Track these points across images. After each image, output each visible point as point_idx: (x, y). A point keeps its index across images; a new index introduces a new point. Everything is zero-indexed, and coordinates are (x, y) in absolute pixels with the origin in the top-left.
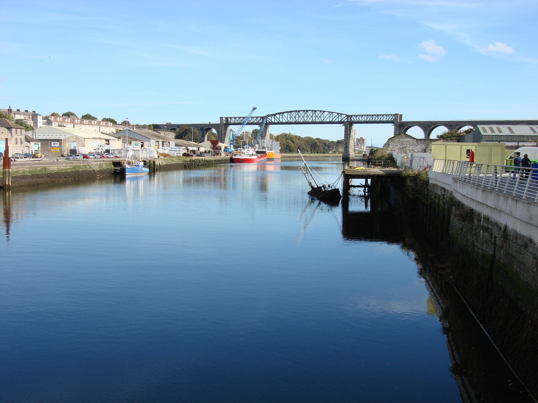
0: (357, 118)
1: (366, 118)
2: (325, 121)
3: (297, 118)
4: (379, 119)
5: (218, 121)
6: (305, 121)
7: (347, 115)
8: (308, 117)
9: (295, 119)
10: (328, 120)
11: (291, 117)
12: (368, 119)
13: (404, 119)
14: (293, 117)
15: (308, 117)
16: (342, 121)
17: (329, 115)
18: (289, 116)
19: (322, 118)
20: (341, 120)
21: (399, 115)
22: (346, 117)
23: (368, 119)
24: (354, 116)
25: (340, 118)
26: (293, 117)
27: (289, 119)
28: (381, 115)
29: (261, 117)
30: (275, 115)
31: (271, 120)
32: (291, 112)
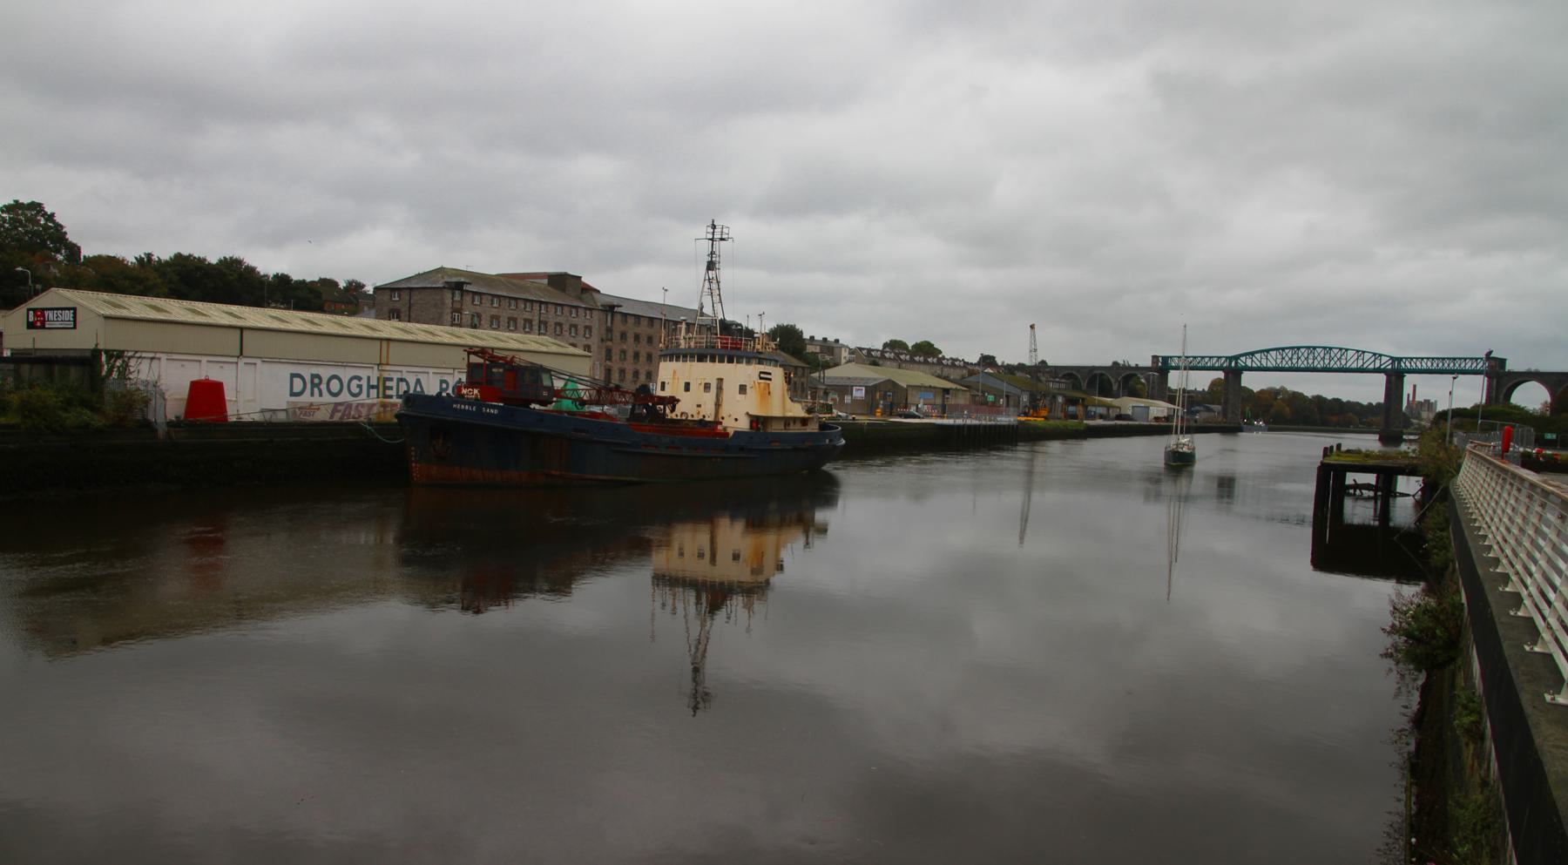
0: (1423, 364)
1: (1429, 364)
3: (1310, 361)
4: (1457, 365)
5: (1148, 363)
7: (1391, 358)
8: (1314, 358)
9: (1290, 362)
10: (1354, 366)
11: (1283, 358)
12: (1435, 365)
13: (1509, 367)
14: (1287, 359)
15: (1314, 358)
17: (1356, 356)
18: (1279, 357)
19: (1343, 362)
21: (1160, 359)
22: (1390, 361)
23: (1435, 365)
24: (1406, 358)
25: (1378, 362)
26: (1287, 359)
27: (1279, 361)
28: (1460, 359)
29: (1227, 358)
30: (1252, 354)
31: (1245, 363)
32: (1283, 349)
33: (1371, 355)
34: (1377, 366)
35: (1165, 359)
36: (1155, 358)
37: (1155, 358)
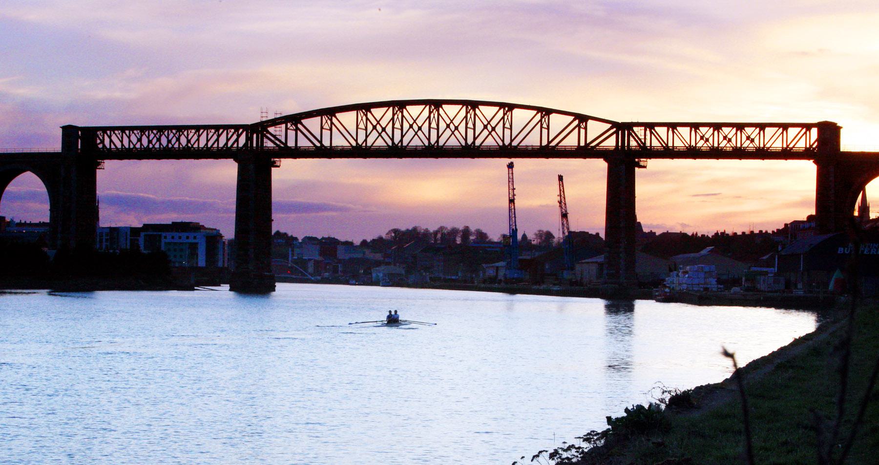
2: (369, 144)
6: (132, 146)
7: (614, 124)
13: (849, 143)
16: (553, 144)
20: (549, 142)
33: (609, 126)
34: (202, 143)
35: (90, 133)
36: (69, 132)
37: (69, 132)
